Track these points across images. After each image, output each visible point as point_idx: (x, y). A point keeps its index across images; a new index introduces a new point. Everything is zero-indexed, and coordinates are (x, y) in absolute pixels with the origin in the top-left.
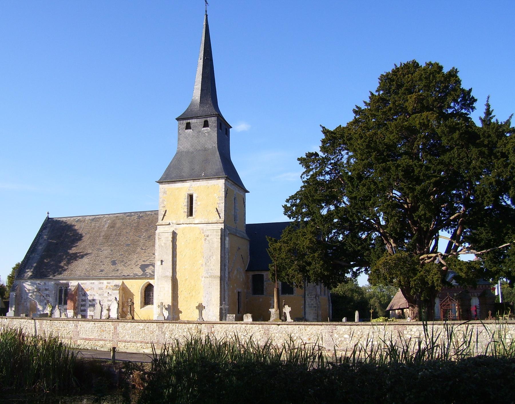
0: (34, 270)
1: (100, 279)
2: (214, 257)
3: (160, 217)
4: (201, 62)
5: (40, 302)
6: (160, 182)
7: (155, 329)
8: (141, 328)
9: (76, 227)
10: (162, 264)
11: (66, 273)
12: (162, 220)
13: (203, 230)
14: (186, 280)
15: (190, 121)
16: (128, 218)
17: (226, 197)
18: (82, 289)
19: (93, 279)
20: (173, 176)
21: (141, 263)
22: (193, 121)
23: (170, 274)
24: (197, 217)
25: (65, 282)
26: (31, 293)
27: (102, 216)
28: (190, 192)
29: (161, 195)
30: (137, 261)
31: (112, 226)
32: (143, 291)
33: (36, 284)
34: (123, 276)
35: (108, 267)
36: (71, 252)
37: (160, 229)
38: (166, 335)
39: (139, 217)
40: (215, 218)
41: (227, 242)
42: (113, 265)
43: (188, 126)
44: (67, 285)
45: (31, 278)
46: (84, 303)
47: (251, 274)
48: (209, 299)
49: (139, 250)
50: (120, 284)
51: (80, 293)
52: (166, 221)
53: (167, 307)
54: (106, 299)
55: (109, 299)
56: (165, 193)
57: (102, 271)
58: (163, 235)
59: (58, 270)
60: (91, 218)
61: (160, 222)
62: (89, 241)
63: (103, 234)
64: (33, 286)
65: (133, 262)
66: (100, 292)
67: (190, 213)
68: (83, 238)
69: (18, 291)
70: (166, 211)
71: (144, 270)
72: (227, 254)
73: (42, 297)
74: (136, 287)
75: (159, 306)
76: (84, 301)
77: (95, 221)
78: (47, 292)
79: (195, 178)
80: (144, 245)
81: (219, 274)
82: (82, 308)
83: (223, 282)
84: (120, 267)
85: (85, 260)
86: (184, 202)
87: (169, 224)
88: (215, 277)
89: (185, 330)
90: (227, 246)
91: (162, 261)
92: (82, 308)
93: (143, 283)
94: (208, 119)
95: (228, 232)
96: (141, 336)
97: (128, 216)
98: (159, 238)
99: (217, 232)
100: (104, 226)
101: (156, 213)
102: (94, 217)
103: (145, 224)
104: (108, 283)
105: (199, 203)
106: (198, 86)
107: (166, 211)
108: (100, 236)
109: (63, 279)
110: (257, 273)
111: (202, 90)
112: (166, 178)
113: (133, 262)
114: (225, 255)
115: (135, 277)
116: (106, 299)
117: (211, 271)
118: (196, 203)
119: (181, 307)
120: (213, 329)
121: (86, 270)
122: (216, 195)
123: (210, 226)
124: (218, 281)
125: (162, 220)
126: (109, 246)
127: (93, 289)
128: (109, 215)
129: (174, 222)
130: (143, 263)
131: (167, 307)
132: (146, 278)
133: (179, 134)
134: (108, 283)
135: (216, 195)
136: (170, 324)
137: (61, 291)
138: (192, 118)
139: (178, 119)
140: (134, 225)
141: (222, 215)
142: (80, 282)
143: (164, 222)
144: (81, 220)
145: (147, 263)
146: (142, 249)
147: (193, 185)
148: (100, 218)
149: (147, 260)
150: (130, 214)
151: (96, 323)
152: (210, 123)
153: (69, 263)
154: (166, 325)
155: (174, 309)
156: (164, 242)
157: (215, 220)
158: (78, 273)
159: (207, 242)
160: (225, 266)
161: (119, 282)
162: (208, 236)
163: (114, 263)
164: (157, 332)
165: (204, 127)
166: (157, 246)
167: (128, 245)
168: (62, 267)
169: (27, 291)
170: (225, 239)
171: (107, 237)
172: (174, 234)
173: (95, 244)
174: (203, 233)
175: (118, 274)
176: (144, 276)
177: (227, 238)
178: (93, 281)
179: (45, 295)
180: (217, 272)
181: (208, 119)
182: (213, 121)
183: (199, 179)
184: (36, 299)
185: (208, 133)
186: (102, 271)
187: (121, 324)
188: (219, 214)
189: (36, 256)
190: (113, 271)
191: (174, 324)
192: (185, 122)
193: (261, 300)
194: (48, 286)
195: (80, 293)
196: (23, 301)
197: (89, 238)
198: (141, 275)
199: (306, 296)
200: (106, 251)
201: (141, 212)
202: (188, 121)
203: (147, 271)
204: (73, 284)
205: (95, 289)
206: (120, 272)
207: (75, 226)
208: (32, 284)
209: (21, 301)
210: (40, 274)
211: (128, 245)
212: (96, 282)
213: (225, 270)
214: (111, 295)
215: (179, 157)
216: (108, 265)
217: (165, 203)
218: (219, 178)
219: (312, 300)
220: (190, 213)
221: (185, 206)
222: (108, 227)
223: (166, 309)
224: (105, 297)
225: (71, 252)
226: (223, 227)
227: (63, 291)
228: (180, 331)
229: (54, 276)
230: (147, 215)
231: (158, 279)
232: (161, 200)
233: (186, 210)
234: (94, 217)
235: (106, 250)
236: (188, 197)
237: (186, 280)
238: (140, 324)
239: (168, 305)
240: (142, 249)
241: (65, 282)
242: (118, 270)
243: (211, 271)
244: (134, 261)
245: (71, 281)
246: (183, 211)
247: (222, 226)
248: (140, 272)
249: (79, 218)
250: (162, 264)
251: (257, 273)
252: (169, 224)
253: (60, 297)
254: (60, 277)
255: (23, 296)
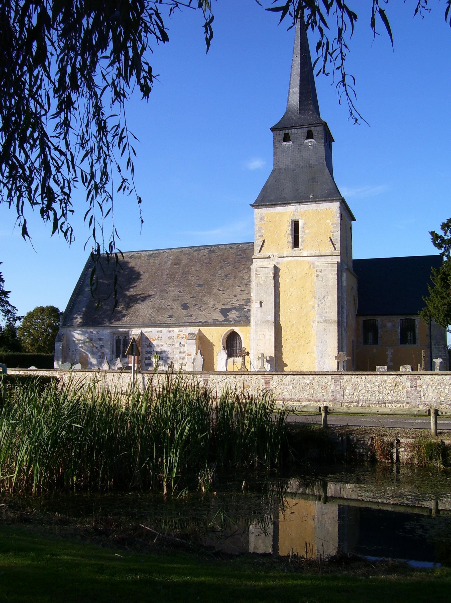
0: (84, 315)
1: (169, 326)
2: (330, 298)
3: (257, 249)
4: (297, 60)
5: (93, 353)
6: (256, 205)
7: (329, 384)
8: (308, 382)
9: (130, 265)
10: (261, 306)
11: (125, 319)
12: (260, 252)
13: (313, 264)
14: (292, 325)
15: (289, 131)
16: (196, 252)
17: (341, 224)
18: (147, 338)
19: (160, 327)
20: (272, 198)
21: (220, 306)
22: (292, 132)
23: (271, 318)
24: (305, 248)
25: (124, 330)
26: (82, 343)
27: (162, 251)
28: (295, 218)
29: (257, 221)
30: (214, 305)
31: (177, 262)
32: (225, 341)
33: (87, 333)
34: (200, 322)
35: (179, 312)
36: (128, 293)
37: (256, 264)
38: (347, 391)
39: (211, 252)
40: (329, 249)
41: (344, 279)
42: (184, 309)
43: (286, 138)
44: (127, 333)
45: (82, 325)
46: (149, 355)
47: (362, 319)
48: (324, 349)
49: (215, 291)
50: (197, 332)
51: (144, 343)
52: (265, 253)
53: (268, 359)
54: (178, 351)
55: (182, 350)
56: (262, 218)
57: (171, 316)
58: (260, 270)
59: (115, 315)
60: (148, 253)
61: (256, 254)
62: (149, 280)
63: (166, 272)
64: (84, 335)
65: (210, 305)
66: (169, 342)
67: (296, 243)
68: (142, 277)
69: (65, 342)
70: (264, 241)
71: (226, 316)
72: (344, 294)
73: (95, 349)
74: (216, 335)
75: (259, 358)
76: (150, 353)
77: (154, 257)
78: (101, 342)
79: (302, 199)
80: (221, 284)
81: (336, 318)
82: (147, 362)
83: (340, 329)
84: (193, 311)
85: (147, 303)
86: (288, 230)
87: (269, 257)
88: (331, 322)
89: (376, 384)
90: (344, 284)
91: (261, 303)
92: (147, 362)
93: (225, 330)
94: (312, 129)
95: (346, 267)
96: (307, 393)
97: (196, 250)
98: (257, 275)
99: (332, 267)
100: (166, 263)
101: (251, 245)
102: (152, 252)
103: (240, 256)
104: (179, 331)
105: (307, 231)
106: (296, 90)
107: (264, 241)
108: (162, 275)
109: (121, 327)
110: (369, 318)
111: (301, 94)
112: (262, 201)
113: (210, 305)
114: (342, 294)
115: (215, 323)
116: (178, 351)
117: (326, 315)
118: (304, 232)
119: (285, 359)
120: (418, 381)
121: (150, 315)
122: (329, 221)
123: (323, 260)
124: (335, 327)
125: (260, 252)
126: (176, 286)
127: (161, 338)
128: (171, 249)
129: (276, 254)
130: (224, 307)
131: (268, 359)
132: (229, 324)
133: (275, 147)
134: (179, 331)
135: (329, 221)
136: (353, 377)
137: (118, 341)
138: (291, 128)
139: (272, 129)
140: (205, 261)
141: (338, 245)
142: (144, 330)
143: (262, 254)
144: (137, 255)
145: (228, 306)
146: (220, 290)
147: (299, 210)
148: (160, 253)
149: (227, 303)
150: (198, 249)
151: (237, 376)
152: (315, 134)
153: (128, 307)
154: (345, 377)
155: (276, 362)
156: (263, 278)
157: (328, 252)
158: (141, 319)
159: (320, 278)
160: (342, 308)
161: (195, 330)
162: (321, 272)
163: (185, 307)
164: (332, 386)
165: (307, 139)
166: (253, 284)
167: (200, 285)
168: (121, 312)
169: (77, 342)
170: (342, 275)
171: (172, 276)
172: (276, 270)
173: (158, 284)
174: (314, 268)
175: (192, 320)
176: (227, 322)
177: (344, 274)
178: (161, 329)
179: (98, 346)
180: (334, 315)
181: (312, 129)
182: (318, 130)
183: (307, 202)
184: (87, 351)
185: (313, 145)
186: (171, 316)
187: (275, 377)
188: (333, 244)
189: (84, 299)
190: (186, 316)
191: (359, 376)
192: (282, 133)
193: (375, 351)
194: (103, 335)
195: (144, 343)
196: (71, 353)
197: (149, 277)
198: (223, 321)
199: (433, 346)
200: (173, 293)
201: (212, 246)
202: (287, 131)
203: (230, 316)
204: (135, 332)
205: (163, 338)
206: (194, 317)
207: (129, 263)
208: (83, 333)
209: (68, 354)
210: (90, 321)
211: (200, 285)
212: (165, 330)
213: (343, 312)
214: (184, 345)
215: (277, 174)
216: (178, 309)
217: (263, 231)
218: (332, 201)
219: (441, 351)
220: (296, 243)
221: (289, 234)
222: (172, 264)
223: (267, 361)
224: (176, 348)
225: (128, 293)
226: (339, 261)
227: (122, 341)
228: (368, 385)
229: (112, 323)
230: (221, 250)
231: (256, 325)
232: (257, 228)
233: (290, 240)
234: (152, 252)
235: (173, 291)
236: (292, 224)
237: (292, 325)
238: (305, 376)
239: (270, 357)
240: (220, 290)
241: (124, 330)
242: (191, 316)
243: (326, 315)
244: (212, 303)
245: (132, 329)
246: (286, 240)
247: (338, 259)
248: (221, 318)
249: (132, 254)
250: (261, 306)
251: (369, 318)
252: (269, 257)
253: (118, 348)
254: (117, 324)
255: (71, 348)
